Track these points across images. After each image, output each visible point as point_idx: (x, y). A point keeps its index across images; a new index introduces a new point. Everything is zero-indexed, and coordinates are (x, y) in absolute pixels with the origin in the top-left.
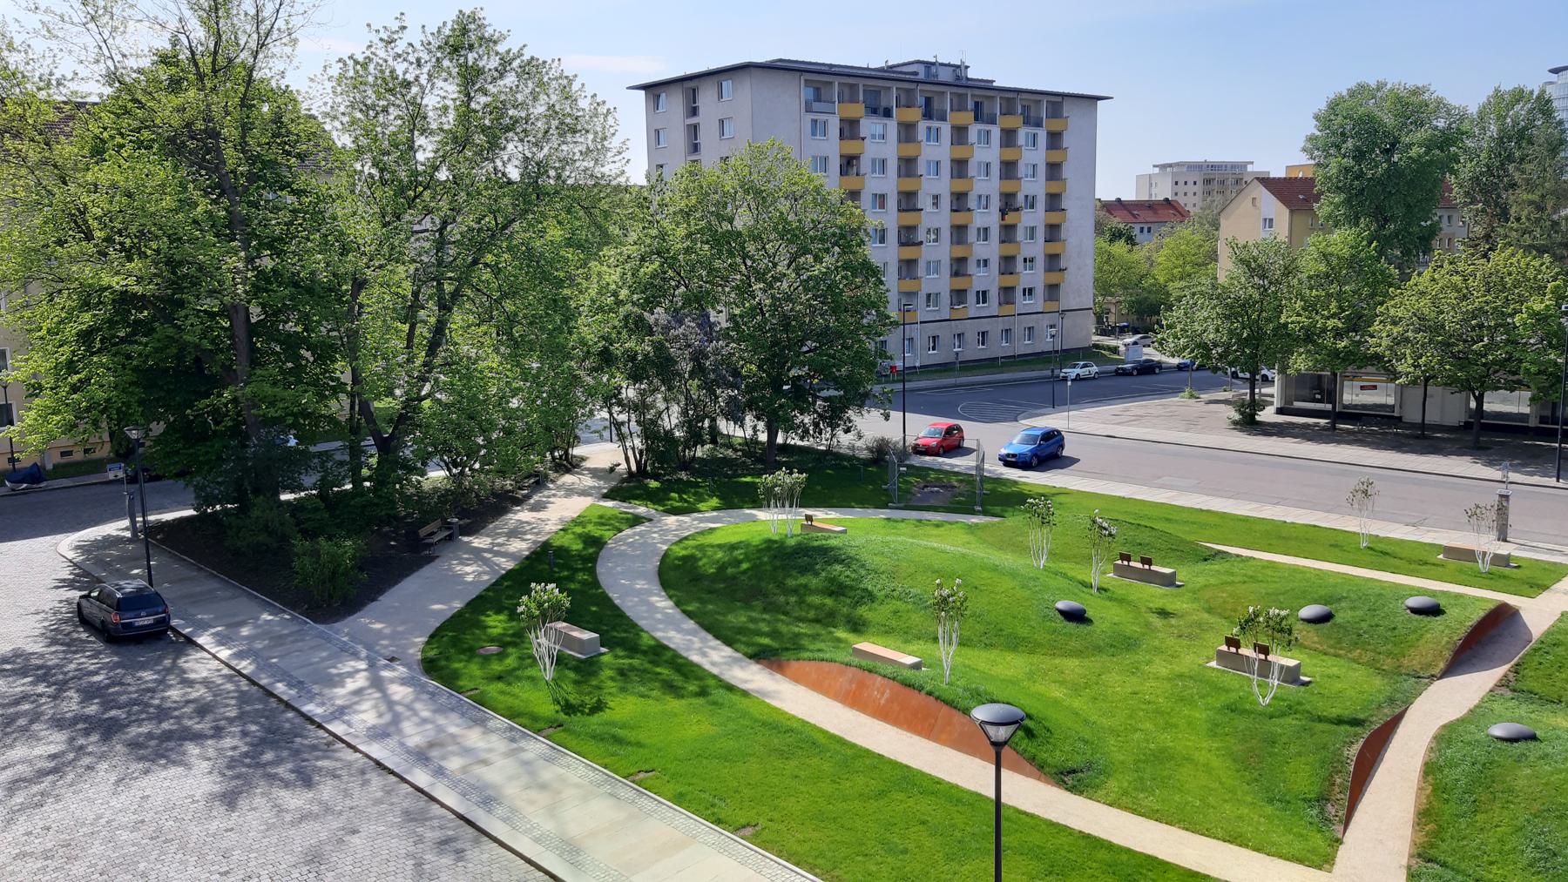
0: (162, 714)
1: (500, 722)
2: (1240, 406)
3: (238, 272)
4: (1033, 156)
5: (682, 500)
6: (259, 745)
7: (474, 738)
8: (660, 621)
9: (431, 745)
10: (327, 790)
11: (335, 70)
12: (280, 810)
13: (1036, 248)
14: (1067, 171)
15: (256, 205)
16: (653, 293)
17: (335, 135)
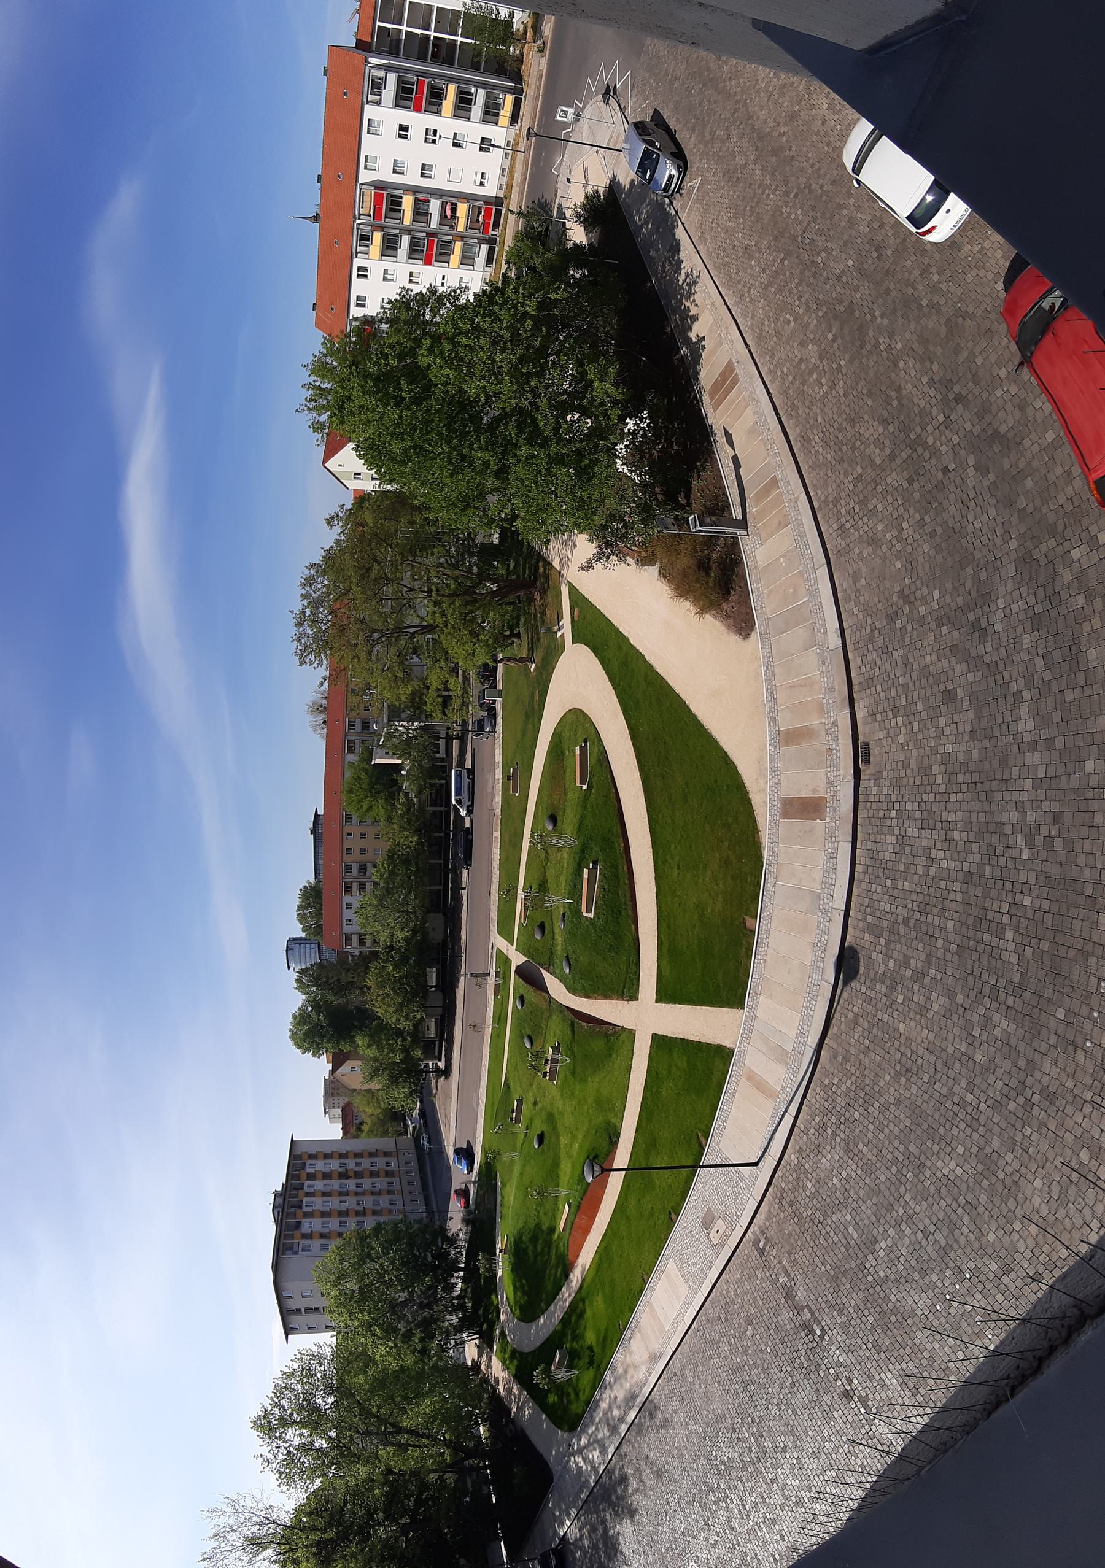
0: (595, 1547)
1: (597, 1395)
2: (438, 1077)
3: (385, 1529)
4: (320, 1165)
5: (492, 1313)
6: (612, 1505)
7: (604, 1405)
8: (551, 1322)
9: (608, 1425)
10: (629, 1471)
11: (284, 1488)
12: (637, 1490)
13: (366, 1163)
14: (328, 1150)
15: (352, 1522)
16: (390, 1331)
17: (315, 1487)
